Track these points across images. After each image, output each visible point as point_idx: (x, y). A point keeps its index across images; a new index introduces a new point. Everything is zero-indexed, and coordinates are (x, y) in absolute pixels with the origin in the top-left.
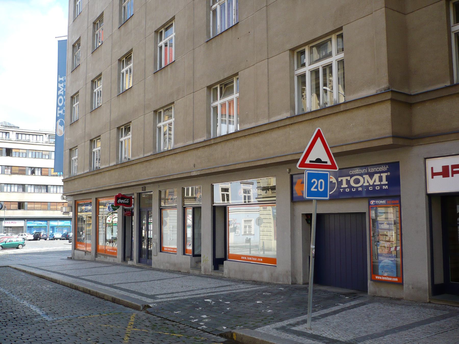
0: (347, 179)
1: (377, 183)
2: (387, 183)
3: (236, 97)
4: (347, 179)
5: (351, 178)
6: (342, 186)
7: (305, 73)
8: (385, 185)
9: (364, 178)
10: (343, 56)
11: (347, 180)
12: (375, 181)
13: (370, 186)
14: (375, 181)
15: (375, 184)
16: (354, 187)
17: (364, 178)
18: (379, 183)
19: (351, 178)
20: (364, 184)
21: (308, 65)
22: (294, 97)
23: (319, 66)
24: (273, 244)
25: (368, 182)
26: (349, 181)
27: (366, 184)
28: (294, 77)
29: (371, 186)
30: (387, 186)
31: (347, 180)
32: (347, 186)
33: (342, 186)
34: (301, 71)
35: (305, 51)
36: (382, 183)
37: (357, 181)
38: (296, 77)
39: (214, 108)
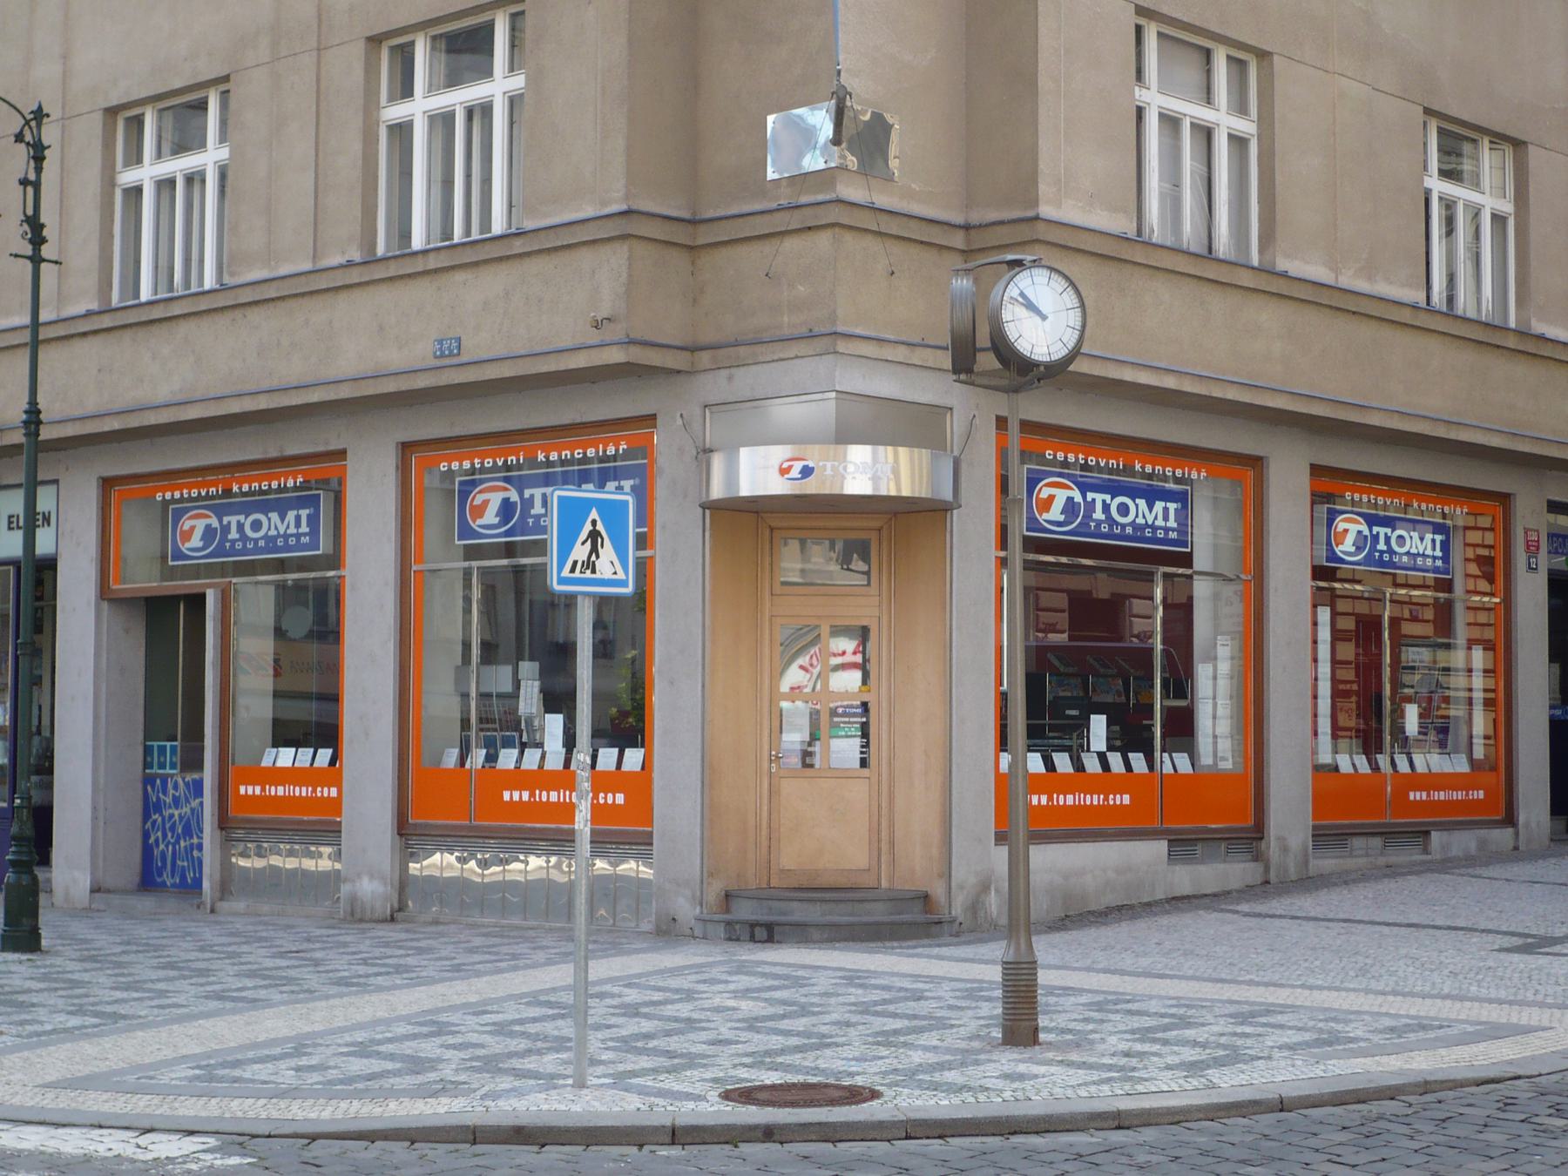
0: (1073, 498)
1: (292, 530)
2: (307, 530)
3: (215, 163)
4: (1073, 498)
5: (1112, 499)
6: (230, 537)
7: (492, 101)
8: (305, 534)
9: (269, 519)
10: (523, 85)
11: (238, 522)
12: (288, 527)
13: (279, 536)
14: (288, 527)
15: (288, 532)
16: (251, 539)
17: (269, 519)
18: (295, 531)
19: (1112, 499)
20: (270, 533)
21: (502, 75)
22: (376, 206)
23: (455, 105)
24: (550, 768)
25: (1144, 517)
26: (243, 525)
27: (273, 532)
28: (112, 195)
29: (1149, 526)
30: (308, 538)
31: (238, 522)
32: (237, 536)
33: (230, 537)
34: (395, 112)
35: (206, 103)
36: (301, 531)
37: (256, 526)
38: (385, 128)
39: (127, 192)
